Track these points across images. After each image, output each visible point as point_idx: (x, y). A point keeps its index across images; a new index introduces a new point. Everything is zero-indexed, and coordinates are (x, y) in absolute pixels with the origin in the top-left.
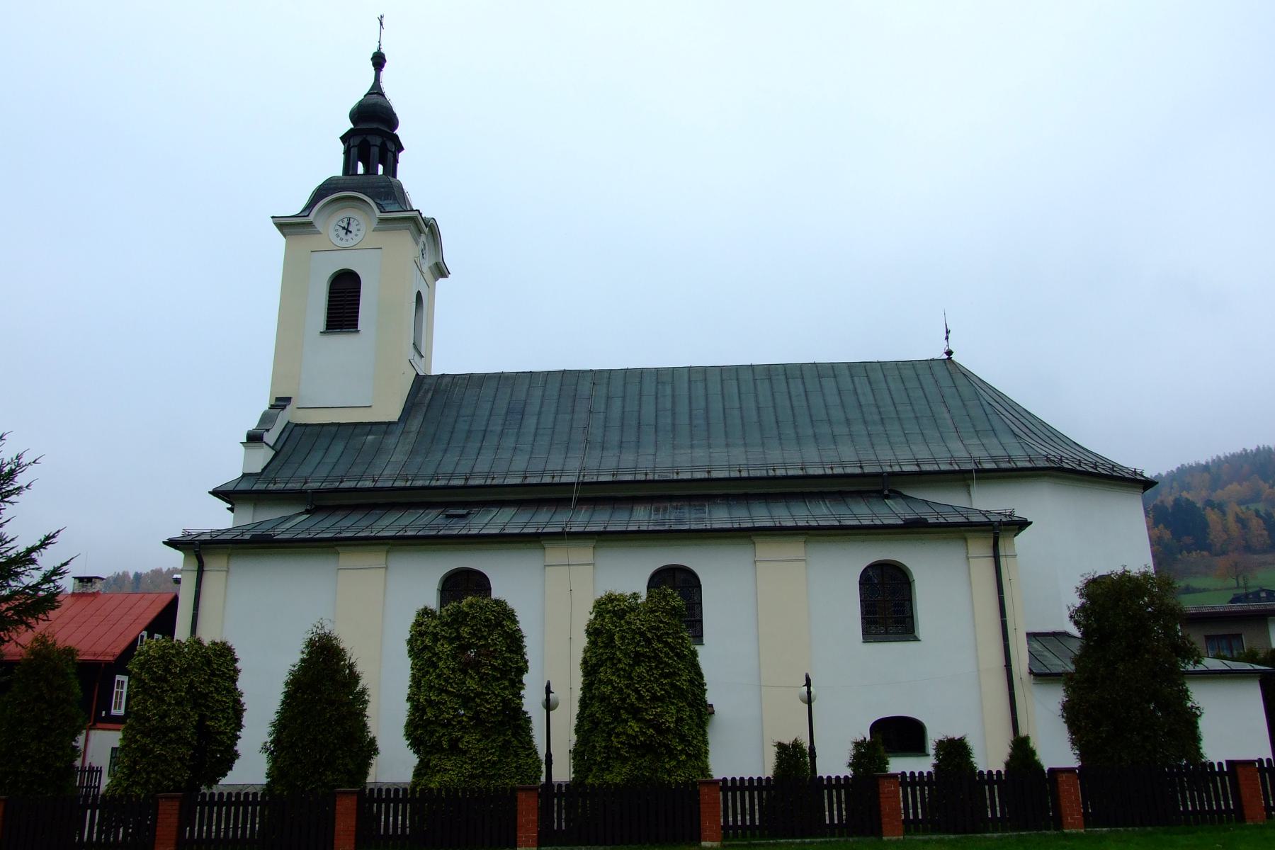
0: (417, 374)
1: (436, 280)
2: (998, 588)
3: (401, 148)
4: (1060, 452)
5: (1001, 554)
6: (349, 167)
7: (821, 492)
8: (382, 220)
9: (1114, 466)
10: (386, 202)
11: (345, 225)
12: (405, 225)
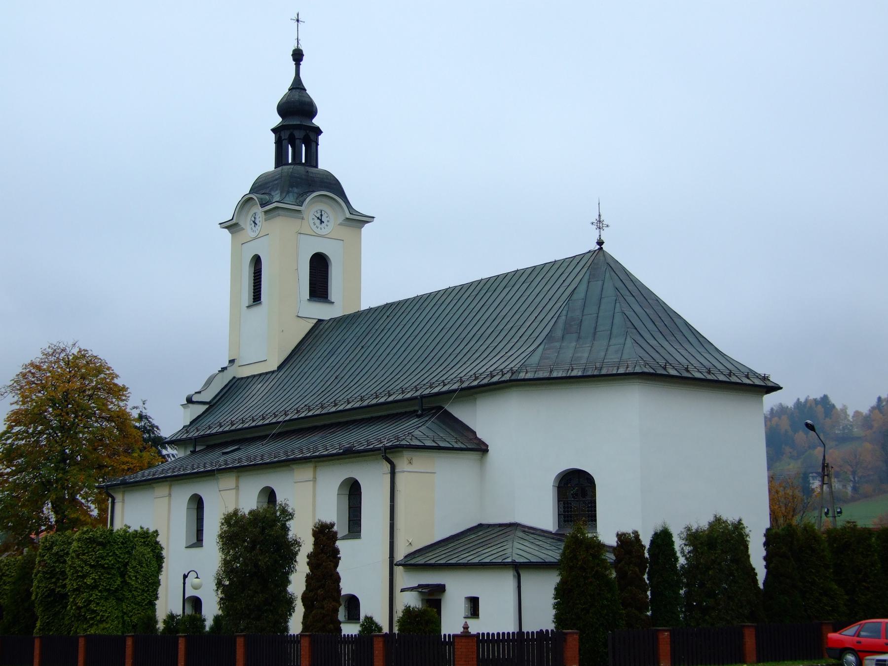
2: (394, 486)
6: (280, 159)
7: (372, 418)
9: (749, 373)
11: (318, 215)
12: (273, 214)
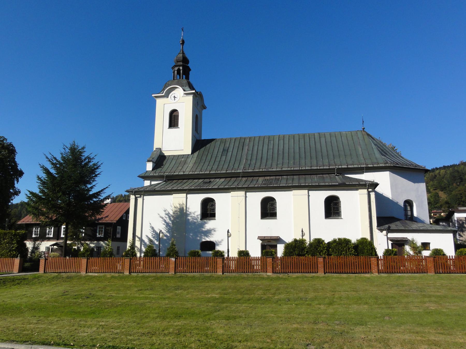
0: (197, 139)
1: (202, 110)
3: (190, 70)
4: (232, 146)
5: (374, 195)
8: (185, 94)
10: (186, 88)
